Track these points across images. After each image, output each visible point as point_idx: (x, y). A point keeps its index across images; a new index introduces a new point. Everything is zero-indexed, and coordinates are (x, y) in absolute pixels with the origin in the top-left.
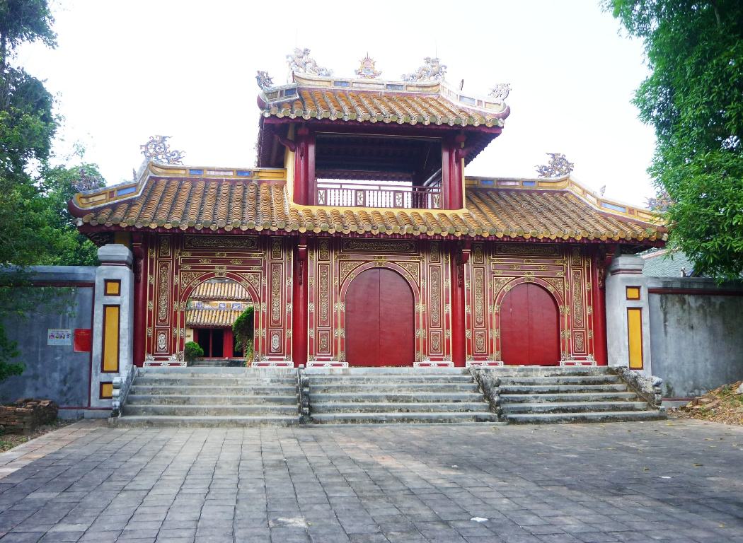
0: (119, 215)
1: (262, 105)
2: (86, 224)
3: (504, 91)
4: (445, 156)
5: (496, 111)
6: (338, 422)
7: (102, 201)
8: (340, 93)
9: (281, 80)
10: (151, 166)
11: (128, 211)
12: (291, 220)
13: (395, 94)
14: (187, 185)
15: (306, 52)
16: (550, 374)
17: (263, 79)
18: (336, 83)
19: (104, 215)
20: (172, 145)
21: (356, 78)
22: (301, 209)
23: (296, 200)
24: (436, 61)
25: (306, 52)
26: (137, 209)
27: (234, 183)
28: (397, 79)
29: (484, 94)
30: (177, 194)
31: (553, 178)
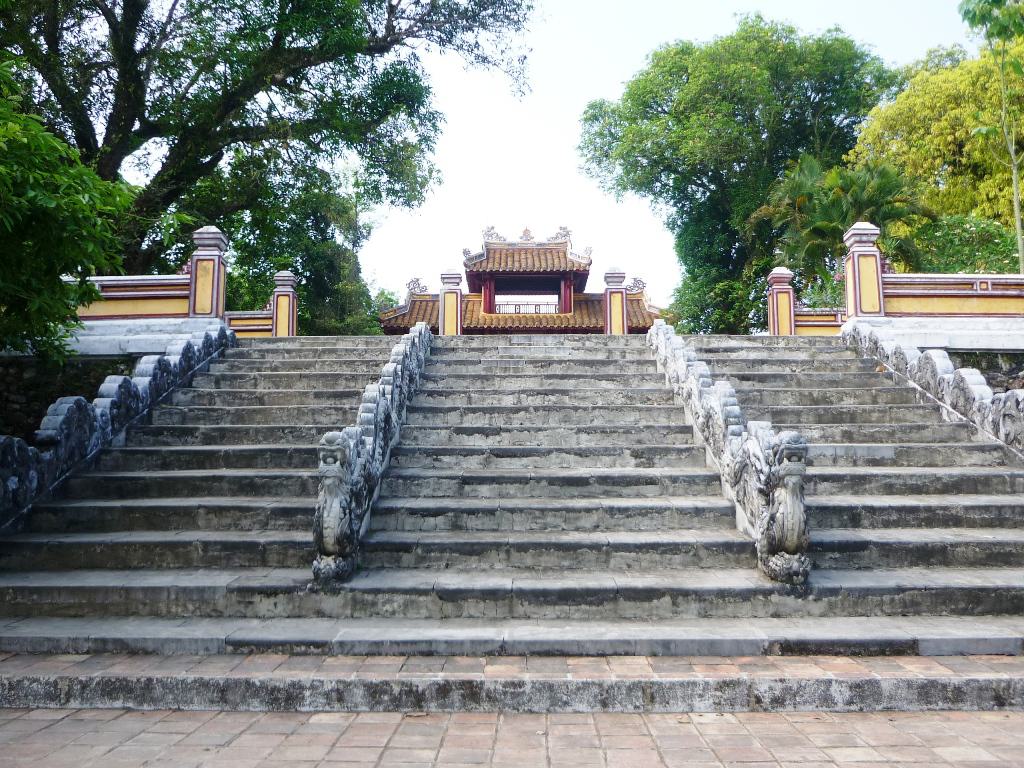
0: (399, 321)
1: (466, 265)
2: (385, 326)
3: (589, 251)
4: (563, 284)
5: (585, 262)
6: (762, 689)
7: (391, 315)
8: (513, 251)
9: (477, 249)
10: (412, 294)
11: (403, 319)
12: (481, 321)
13: (543, 250)
14: (430, 304)
15: (493, 228)
16: (487, 354)
17: (466, 252)
18: (509, 245)
19: (393, 321)
20: (422, 283)
21: (519, 241)
22: (487, 316)
23: (485, 311)
24: (564, 229)
25: (493, 228)
26: (407, 318)
27: (507, 250)
28: (545, 241)
29: (582, 253)
30: (426, 310)
31: (634, 292)
